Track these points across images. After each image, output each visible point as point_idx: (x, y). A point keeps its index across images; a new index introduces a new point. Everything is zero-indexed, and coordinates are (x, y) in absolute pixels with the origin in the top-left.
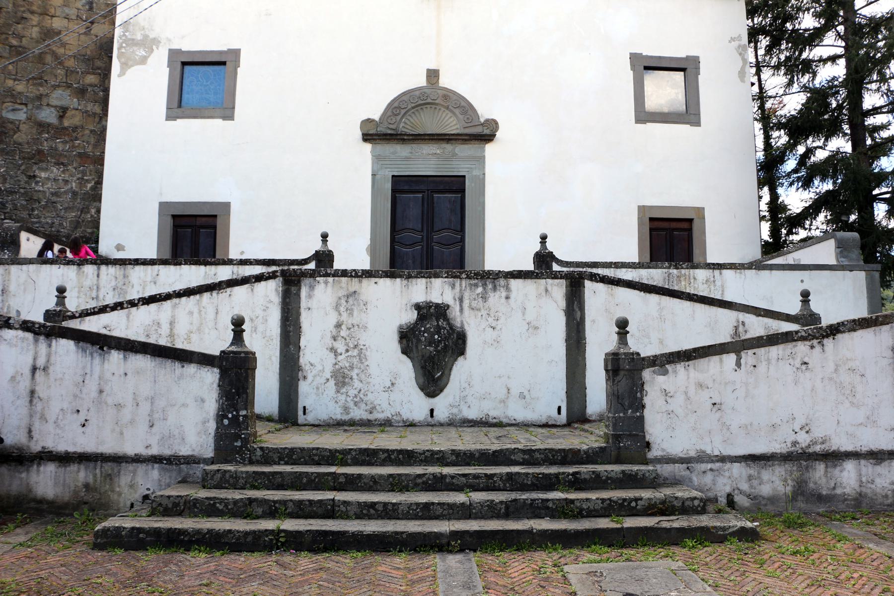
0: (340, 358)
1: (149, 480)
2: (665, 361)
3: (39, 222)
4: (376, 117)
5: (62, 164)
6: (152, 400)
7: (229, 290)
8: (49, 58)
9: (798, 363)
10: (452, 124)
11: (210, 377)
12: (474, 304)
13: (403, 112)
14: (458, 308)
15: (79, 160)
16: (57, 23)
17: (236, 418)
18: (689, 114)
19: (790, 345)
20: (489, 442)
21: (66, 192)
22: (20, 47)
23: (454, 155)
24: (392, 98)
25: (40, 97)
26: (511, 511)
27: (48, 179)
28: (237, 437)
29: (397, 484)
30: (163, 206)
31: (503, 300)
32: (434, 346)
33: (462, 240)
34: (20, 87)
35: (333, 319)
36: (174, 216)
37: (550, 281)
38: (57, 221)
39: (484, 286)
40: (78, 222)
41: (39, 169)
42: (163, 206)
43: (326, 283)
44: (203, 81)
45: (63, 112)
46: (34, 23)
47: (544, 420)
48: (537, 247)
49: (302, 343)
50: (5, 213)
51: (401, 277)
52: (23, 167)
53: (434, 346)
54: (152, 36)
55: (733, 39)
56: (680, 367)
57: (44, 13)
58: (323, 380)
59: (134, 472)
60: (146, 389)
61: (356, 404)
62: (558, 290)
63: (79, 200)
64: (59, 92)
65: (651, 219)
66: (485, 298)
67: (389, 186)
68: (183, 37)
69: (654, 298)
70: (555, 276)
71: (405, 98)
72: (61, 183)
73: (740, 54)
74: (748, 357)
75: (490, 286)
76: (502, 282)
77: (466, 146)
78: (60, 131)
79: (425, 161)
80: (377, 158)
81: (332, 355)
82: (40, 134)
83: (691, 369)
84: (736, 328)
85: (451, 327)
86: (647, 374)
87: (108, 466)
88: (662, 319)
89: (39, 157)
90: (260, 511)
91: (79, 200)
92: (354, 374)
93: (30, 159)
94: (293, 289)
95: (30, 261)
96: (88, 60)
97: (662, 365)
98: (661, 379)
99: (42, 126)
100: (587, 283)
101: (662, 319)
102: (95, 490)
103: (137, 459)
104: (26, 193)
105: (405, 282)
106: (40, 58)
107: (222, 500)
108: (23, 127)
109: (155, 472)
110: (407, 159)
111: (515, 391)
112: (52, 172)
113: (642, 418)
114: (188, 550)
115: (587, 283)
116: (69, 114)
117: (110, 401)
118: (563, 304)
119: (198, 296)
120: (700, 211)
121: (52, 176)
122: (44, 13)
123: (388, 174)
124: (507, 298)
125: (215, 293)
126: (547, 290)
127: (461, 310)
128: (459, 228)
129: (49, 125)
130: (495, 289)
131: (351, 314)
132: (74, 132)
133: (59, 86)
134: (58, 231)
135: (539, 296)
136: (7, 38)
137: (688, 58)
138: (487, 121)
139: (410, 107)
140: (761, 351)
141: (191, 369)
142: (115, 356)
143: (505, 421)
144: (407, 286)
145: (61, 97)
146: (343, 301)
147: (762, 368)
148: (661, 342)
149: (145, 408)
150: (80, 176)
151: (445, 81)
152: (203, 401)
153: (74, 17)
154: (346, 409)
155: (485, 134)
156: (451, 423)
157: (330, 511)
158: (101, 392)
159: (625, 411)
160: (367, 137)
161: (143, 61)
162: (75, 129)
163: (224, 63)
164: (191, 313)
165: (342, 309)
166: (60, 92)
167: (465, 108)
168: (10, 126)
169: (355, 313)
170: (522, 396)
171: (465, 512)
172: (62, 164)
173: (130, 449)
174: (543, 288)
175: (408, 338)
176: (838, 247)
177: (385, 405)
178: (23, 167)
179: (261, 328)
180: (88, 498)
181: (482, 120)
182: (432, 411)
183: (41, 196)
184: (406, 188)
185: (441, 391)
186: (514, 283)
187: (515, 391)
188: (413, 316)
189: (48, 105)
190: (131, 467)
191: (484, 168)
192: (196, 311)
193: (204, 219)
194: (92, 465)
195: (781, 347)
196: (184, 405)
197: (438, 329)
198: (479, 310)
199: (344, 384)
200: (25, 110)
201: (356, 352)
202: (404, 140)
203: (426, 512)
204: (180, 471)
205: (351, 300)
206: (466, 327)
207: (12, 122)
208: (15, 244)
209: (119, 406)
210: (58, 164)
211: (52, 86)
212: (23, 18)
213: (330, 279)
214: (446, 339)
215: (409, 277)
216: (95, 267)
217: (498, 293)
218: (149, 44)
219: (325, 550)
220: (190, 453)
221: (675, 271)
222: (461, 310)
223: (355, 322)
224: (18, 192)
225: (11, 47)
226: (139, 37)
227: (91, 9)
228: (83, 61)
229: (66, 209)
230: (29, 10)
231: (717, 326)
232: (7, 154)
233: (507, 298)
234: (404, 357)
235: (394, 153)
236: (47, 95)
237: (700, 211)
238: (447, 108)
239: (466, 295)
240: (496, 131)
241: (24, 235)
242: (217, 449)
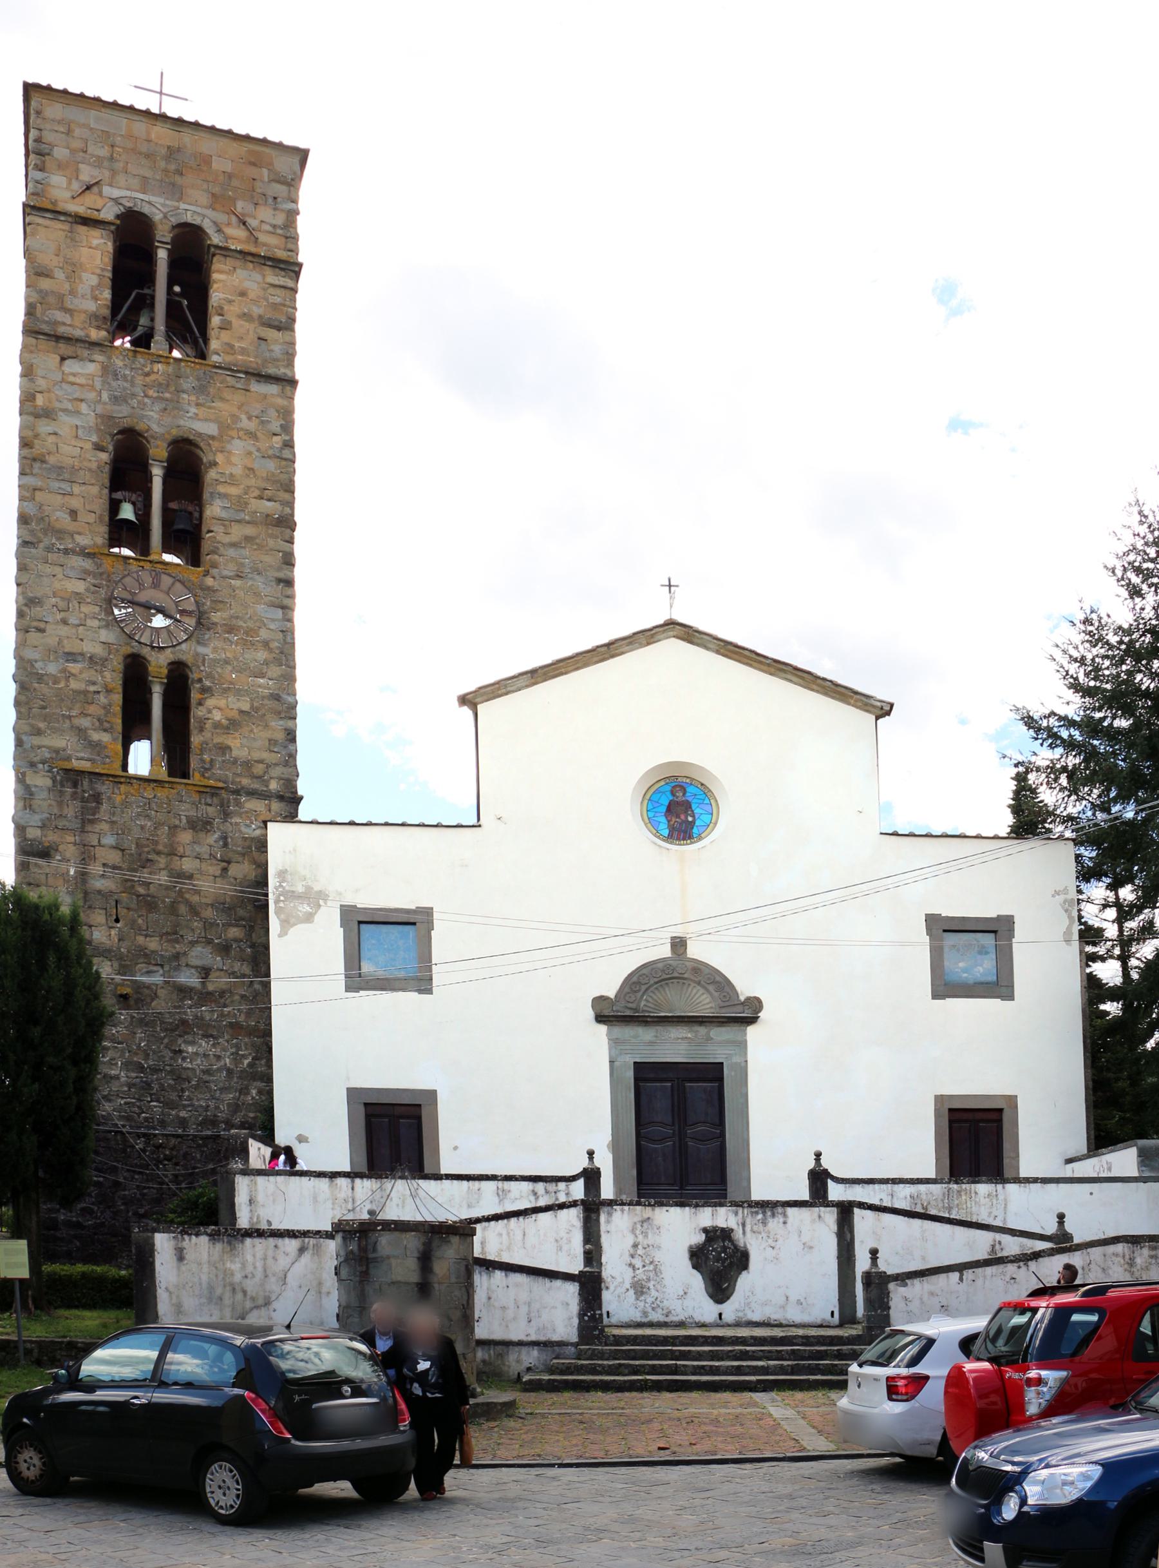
0: (637, 1272)
1: (531, 1357)
2: (903, 1278)
3: (192, 1105)
4: (612, 994)
5: (212, 1036)
6: (529, 1304)
7: (534, 1216)
8: (183, 909)
9: (1008, 1278)
10: (704, 1003)
11: (573, 1289)
12: (755, 1228)
13: (644, 988)
14: (741, 1231)
15: (230, 1031)
16: (188, 865)
17: (593, 1316)
18: (1000, 986)
19: (1002, 1266)
20: (778, 1333)
21: (219, 1070)
22: (148, 895)
23: (709, 1039)
24: (630, 972)
25: (177, 956)
26: (794, 1370)
27: (196, 1054)
28: (596, 1328)
29: (714, 1356)
30: (353, 1094)
31: (781, 1225)
32: (720, 1262)
33: (722, 1135)
34: (153, 944)
35: (630, 1240)
36: (366, 1104)
37: (822, 1209)
38: (212, 1104)
39: (764, 1213)
40: (237, 1105)
41: (185, 1042)
42: (353, 1094)
43: (622, 1211)
44: (389, 946)
45: (205, 972)
46: (162, 866)
47: (819, 1322)
48: (811, 1164)
49: (604, 1260)
50: (151, 1095)
51: (689, 1206)
52: (166, 1041)
53: (720, 1262)
54: (317, 888)
55: (1057, 893)
56: (917, 1281)
57: (172, 853)
58: (624, 1290)
59: (520, 1352)
60: (524, 1296)
61: (653, 1309)
62: (830, 1216)
63: (235, 1080)
64: (199, 949)
65: (950, 1110)
66: (764, 1223)
67: (630, 1074)
68: (357, 891)
69: (917, 1222)
70: (828, 1204)
71: (644, 971)
72: (213, 1060)
73: (1066, 911)
74: (968, 1274)
75: (769, 1213)
76: (780, 1210)
77: (723, 1029)
78: (205, 997)
79: (674, 1047)
80: (614, 1042)
81: (631, 1270)
82: (182, 1000)
83: (925, 1284)
84: (993, 1246)
85: (736, 1247)
86: (892, 1286)
87: (499, 1348)
88: (924, 1239)
89: (183, 1028)
90: (626, 1371)
91: (235, 1080)
92: (651, 1285)
93: (173, 1030)
94: (594, 1216)
95: (260, 1173)
96: (229, 908)
97: (903, 1280)
98: (902, 1289)
99: (183, 991)
100: (856, 1211)
101: (924, 1239)
102: (490, 1364)
103: (521, 1344)
104: (172, 1072)
105: (693, 1210)
106: (173, 909)
107: (600, 1365)
108: (162, 993)
109: (535, 1352)
110: (651, 1043)
111: (793, 1299)
112: (200, 1046)
113: (888, 1316)
114: (588, 1391)
115: (856, 1211)
116: (213, 975)
117: (496, 1304)
118: (835, 1228)
119: (506, 1221)
120: (1012, 1100)
121: (201, 1050)
122: (172, 853)
123: (630, 1060)
124: (785, 1223)
125: (521, 1218)
126: (820, 1217)
127: (744, 1233)
128: (717, 1121)
129: (191, 989)
130: (773, 1215)
131: (646, 1236)
132: (221, 997)
133: (197, 942)
134: (215, 1116)
135: (813, 1221)
136: (133, 887)
137: (999, 918)
138: (748, 999)
139: (652, 982)
140: (979, 1270)
141: (558, 1283)
142: (499, 1274)
143: (784, 1322)
144: (695, 1213)
145: (201, 955)
146: (639, 1226)
147: (979, 1282)
148: (923, 1258)
149: (524, 1309)
150: (233, 1050)
151: (694, 951)
152: (567, 1304)
153: (207, 856)
154: (645, 1314)
155: (746, 1014)
156: (738, 1324)
157: (675, 1370)
158: (489, 1298)
159: (876, 1311)
160: (600, 1019)
161: (309, 918)
162: (222, 993)
163: (414, 924)
164: (500, 1235)
165: (638, 1232)
166: (199, 949)
167: (719, 983)
168: (146, 991)
169: (650, 1236)
170: (799, 1303)
171: (765, 1371)
172: (212, 1036)
173: (515, 1337)
174: (816, 1215)
175: (697, 1256)
176: (1139, 1156)
177: (679, 1310)
178: (166, 1041)
179: (565, 1248)
180: (487, 1369)
181: (742, 998)
182: (720, 1315)
183: (190, 1074)
184: (652, 1076)
185: (728, 1298)
186: (790, 1211)
187: (793, 1299)
188: (702, 1238)
189: (187, 965)
190: (517, 1349)
191: (746, 1054)
192: (504, 1233)
193: (403, 1108)
194: (486, 1347)
195: (995, 1268)
196: (554, 1307)
197: (724, 1249)
198: (760, 1233)
199: (642, 1293)
200: (161, 972)
201: (651, 1267)
202: (647, 1022)
203: (738, 1371)
204: (554, 1351)
205: (645, 1225)
206: (749, 1246)
207: (148, 987)
208: (244, 1152)
209: (504, 1308)
210: (206, 1036)
211: (190, 942)
212: (149, 860)
213: (626, 1208)
214: (731, 1257)
215: (697, 1206)
216: (349, 1180)
217: (776, 1220)
218: (316, 898)
219: (677, 1391)
220: (559, 1339)
221: (955, 1186)
222: (744, 1233)
223: (650, 1243)
224: (164, 1069)
225: (138, 896)
226: (300, 888)
227: (226, 845)
228: (223, 911)
229: (221, 1090)
230: (154, 850)
231: (979, 1244)
232: (146, 1025)
233: (785, 1223)
234: (695, 1271)
235: (636, 1037)
236: (185, 953)
237: (1012, 1100)
238: (699, 983)
239: (748, 1221)
240: (760, 1011)
241: (251, 1141)
242: (580, 1335)
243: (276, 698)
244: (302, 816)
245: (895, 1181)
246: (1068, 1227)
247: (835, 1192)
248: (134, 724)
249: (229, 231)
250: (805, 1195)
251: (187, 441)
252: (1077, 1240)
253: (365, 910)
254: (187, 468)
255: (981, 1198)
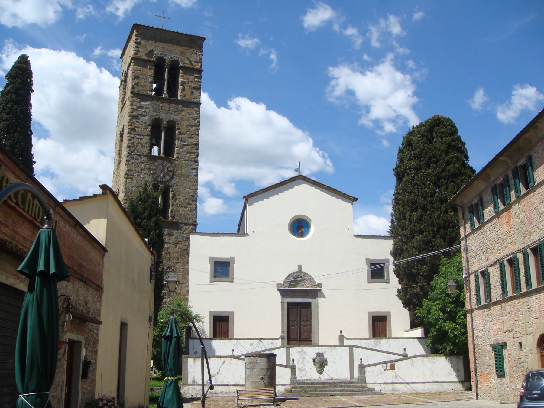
10: (307, 286)
32: (321, 363)
53: (321, 363)
181: (317, 283)
243: (193, 196)
244: (198, 231)
245: (361, 339)
246: (407, 352)
247: (346, 342)
248: (155, 141)
249: (185, 62)
250: (338, 344)
251: (173, 121)
252: (409, 356)
253: (216, 258)
254: (171, 128)
255: (383, 344)
